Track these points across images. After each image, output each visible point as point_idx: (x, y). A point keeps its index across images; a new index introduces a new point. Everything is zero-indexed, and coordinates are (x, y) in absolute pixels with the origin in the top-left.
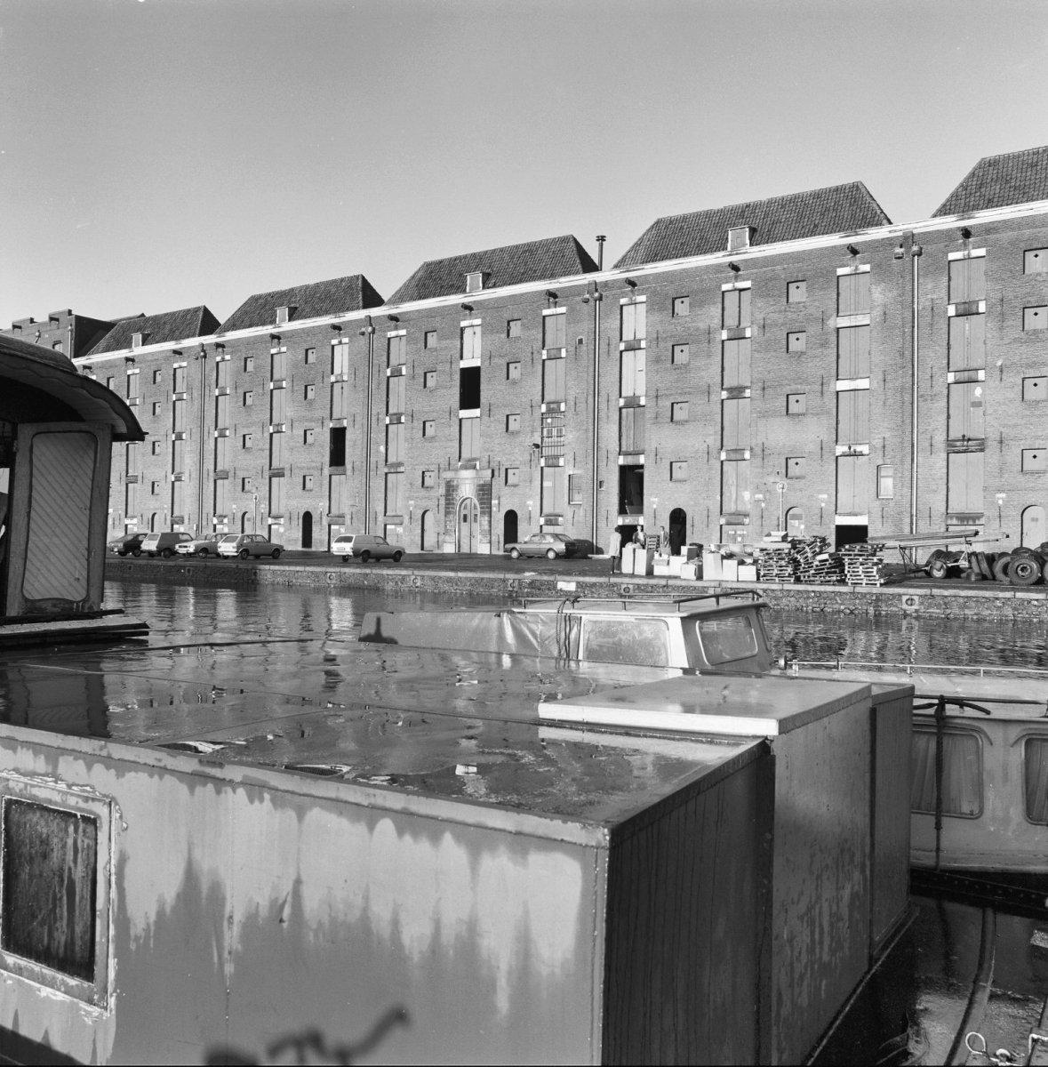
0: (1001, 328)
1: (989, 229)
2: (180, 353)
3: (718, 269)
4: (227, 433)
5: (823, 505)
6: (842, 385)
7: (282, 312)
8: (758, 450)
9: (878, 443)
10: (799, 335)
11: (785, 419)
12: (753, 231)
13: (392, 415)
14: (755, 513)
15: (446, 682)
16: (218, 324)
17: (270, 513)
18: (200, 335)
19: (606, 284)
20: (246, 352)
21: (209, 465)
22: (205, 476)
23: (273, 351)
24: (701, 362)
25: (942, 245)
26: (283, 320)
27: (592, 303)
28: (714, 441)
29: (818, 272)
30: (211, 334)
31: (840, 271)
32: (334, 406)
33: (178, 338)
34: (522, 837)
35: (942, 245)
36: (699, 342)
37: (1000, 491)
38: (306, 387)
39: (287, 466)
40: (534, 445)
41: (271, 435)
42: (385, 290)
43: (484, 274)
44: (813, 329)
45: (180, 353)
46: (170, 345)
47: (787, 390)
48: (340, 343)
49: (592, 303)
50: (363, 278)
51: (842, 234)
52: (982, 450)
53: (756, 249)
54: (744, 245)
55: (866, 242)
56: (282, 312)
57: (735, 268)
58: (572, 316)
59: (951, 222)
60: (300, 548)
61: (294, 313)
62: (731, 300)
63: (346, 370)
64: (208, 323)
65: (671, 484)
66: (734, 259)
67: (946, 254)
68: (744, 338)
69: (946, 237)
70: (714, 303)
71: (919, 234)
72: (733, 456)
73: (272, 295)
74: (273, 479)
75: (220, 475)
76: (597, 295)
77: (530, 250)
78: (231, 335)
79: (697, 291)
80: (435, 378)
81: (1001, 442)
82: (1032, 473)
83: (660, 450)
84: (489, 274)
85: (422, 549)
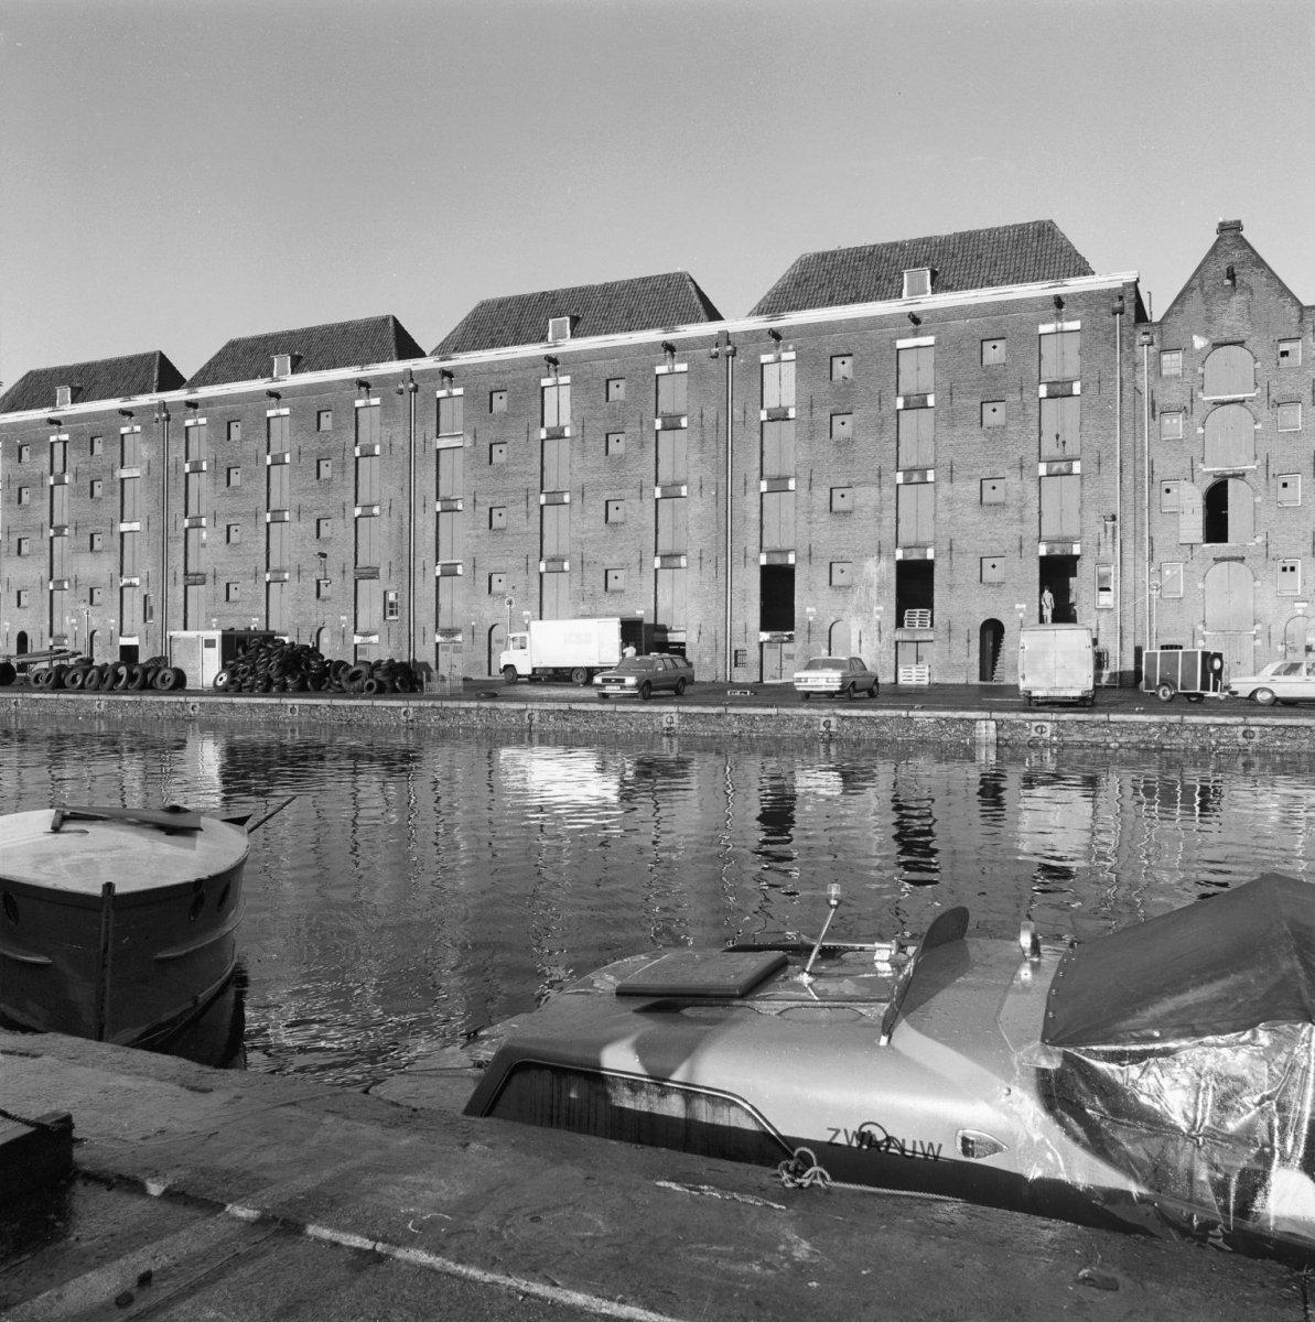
0: (215, 484)
1: (209, 402)
2: (59, 423)
3: (531, 363)
4: (287, 516)
5: (811, 618)
6: (124, 527)
7: (63, 393)
8: (73, 581)
9: (144, 576)
10: (996, 405)
11: (90, 555)
12: (575, 321)
13: (274, 511)
14: (71, 636)
15: (534, 863)
16: (184, 381)
17: (356, 628)
18: (160, 390)
19: (423, 373)
20: (227, 419)
21: (177, 561)
22: (171, 578)
23: (441, 394)
24: (37, 504)
25: (181, 413)
26: (65, 403)
27: (407, 394)
28: (45, 573)
29: (636, 368)
30: (178, 388)
31: (1043, 329)
32: (272, 495)
33: (364, 363)
34: (534, 1072)
35: (181, 413)
36: (35, 485)
37: (214, 616)
38: (318, 461)
39: (211, 572)
40: (320, 554)
41: (186, 530)
42: (426, 339)
43: (293, 358)
44: (106, 478)
45: (59, 423)
46: (115, 404)
47: (607, 495)
48: (778, 360)
49: (407, 394)
50: (394, 319)
51: (121, 399)
52: (204, 584)
53: (75, 406)
54: (925, 292)
55: (612, 348)
56: (63, 393)
57: (915, 319)
58: (697, 375)
59: (761, 323)
60: (976, 681)
61: (298, 362)
62: (58, 449)
63: (565, 420)
64: (169, 377)
65: (18, 610)
66: (552, 352)
67: (184, 420)
68: (789, 419)
69: (753, 336)
70: (45, 452)
71: (171, 403)
72: (552, 566)
73: (266, 339)
74: (360, 582)
75: (192, 579)
76: (411, 385)
77: (344, 329)
78: (204, 392)
79: (873, 346)
80: (504, 452)
81: (215, 577)
82: (991, 584)
83: (11, 580)
84: (300, 358)
85: (490, 674)
